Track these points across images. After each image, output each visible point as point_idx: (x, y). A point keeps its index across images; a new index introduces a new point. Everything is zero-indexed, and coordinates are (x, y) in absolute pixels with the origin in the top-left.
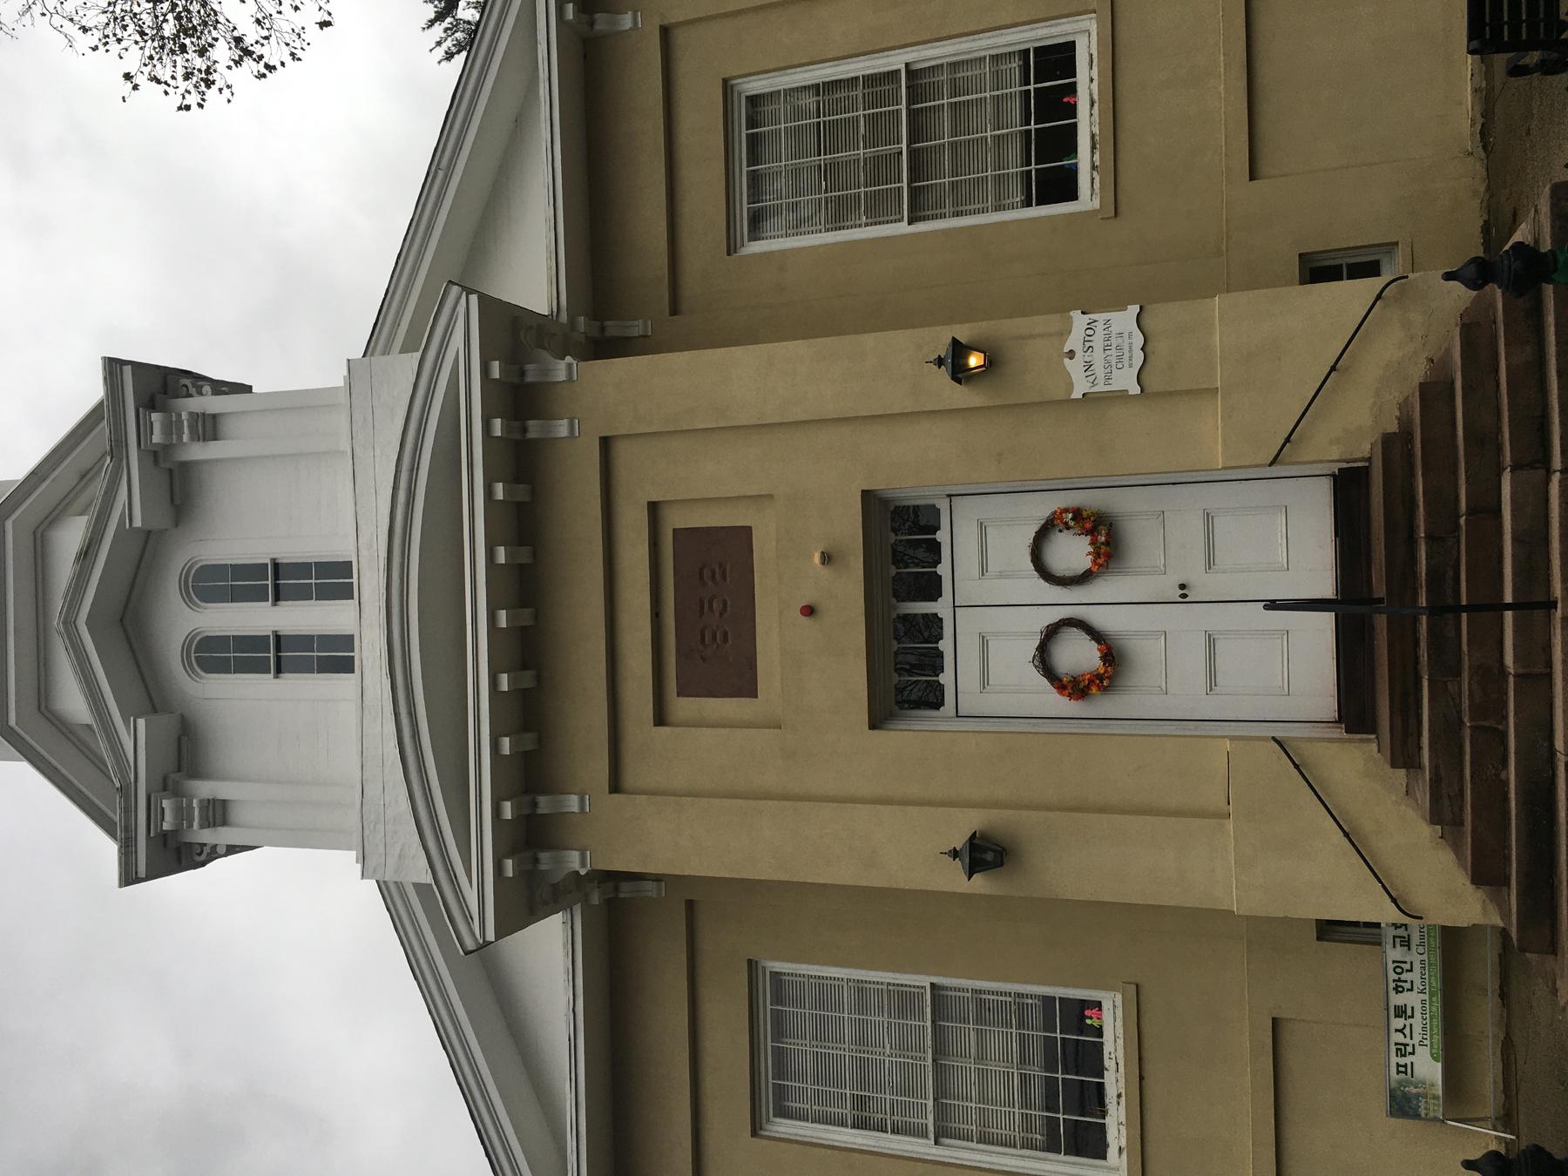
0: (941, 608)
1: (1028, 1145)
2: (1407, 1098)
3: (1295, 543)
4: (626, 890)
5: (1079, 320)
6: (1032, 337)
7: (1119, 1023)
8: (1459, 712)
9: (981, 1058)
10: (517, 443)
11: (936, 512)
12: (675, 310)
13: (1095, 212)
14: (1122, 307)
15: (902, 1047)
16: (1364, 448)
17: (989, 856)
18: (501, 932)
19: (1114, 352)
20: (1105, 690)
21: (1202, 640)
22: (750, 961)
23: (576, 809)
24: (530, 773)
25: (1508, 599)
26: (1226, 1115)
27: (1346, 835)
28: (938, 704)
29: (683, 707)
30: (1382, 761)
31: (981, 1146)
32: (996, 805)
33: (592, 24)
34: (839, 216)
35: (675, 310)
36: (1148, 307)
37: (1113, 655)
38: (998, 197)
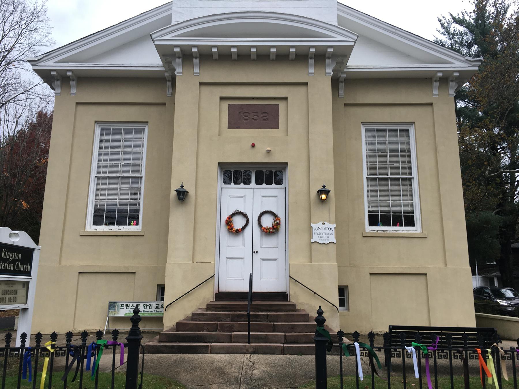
0: (253, 184)
1: (96, 203)
2: (114, 307)
3: (267, 282)
4: (169, 84)
5: (333, 226)
6: (329, 213)
7: (133, 230)
8: (221, 321)
9: (121, 190)
10: (307, 56)
11: (280, 184)
12: (346, 105)
13: (365, 231)
14: (336, 238)
15: (123, 167)
16: (293, 300)
17: (181, 196)
18: (157, 46)
19: (323, 235)
20: (228, 230)
21: (241, 257)
22: (148, 122)
23: (195, 71)
24: (206, 57)
25: (251, 333)
26: (110, 257)
27: (188, 292)
28: (225, 183)
29: (225, 105)
30: (209, 302)
31: (95, 190)
32: (196, 199)
33: (436, 81)
34: (371, 155)
35: (346, 105)
36: (335, 245)
37: (238, 232)
38: (372, 203)
